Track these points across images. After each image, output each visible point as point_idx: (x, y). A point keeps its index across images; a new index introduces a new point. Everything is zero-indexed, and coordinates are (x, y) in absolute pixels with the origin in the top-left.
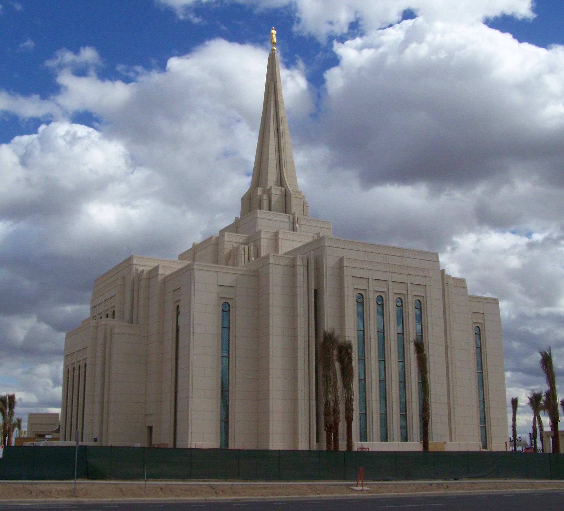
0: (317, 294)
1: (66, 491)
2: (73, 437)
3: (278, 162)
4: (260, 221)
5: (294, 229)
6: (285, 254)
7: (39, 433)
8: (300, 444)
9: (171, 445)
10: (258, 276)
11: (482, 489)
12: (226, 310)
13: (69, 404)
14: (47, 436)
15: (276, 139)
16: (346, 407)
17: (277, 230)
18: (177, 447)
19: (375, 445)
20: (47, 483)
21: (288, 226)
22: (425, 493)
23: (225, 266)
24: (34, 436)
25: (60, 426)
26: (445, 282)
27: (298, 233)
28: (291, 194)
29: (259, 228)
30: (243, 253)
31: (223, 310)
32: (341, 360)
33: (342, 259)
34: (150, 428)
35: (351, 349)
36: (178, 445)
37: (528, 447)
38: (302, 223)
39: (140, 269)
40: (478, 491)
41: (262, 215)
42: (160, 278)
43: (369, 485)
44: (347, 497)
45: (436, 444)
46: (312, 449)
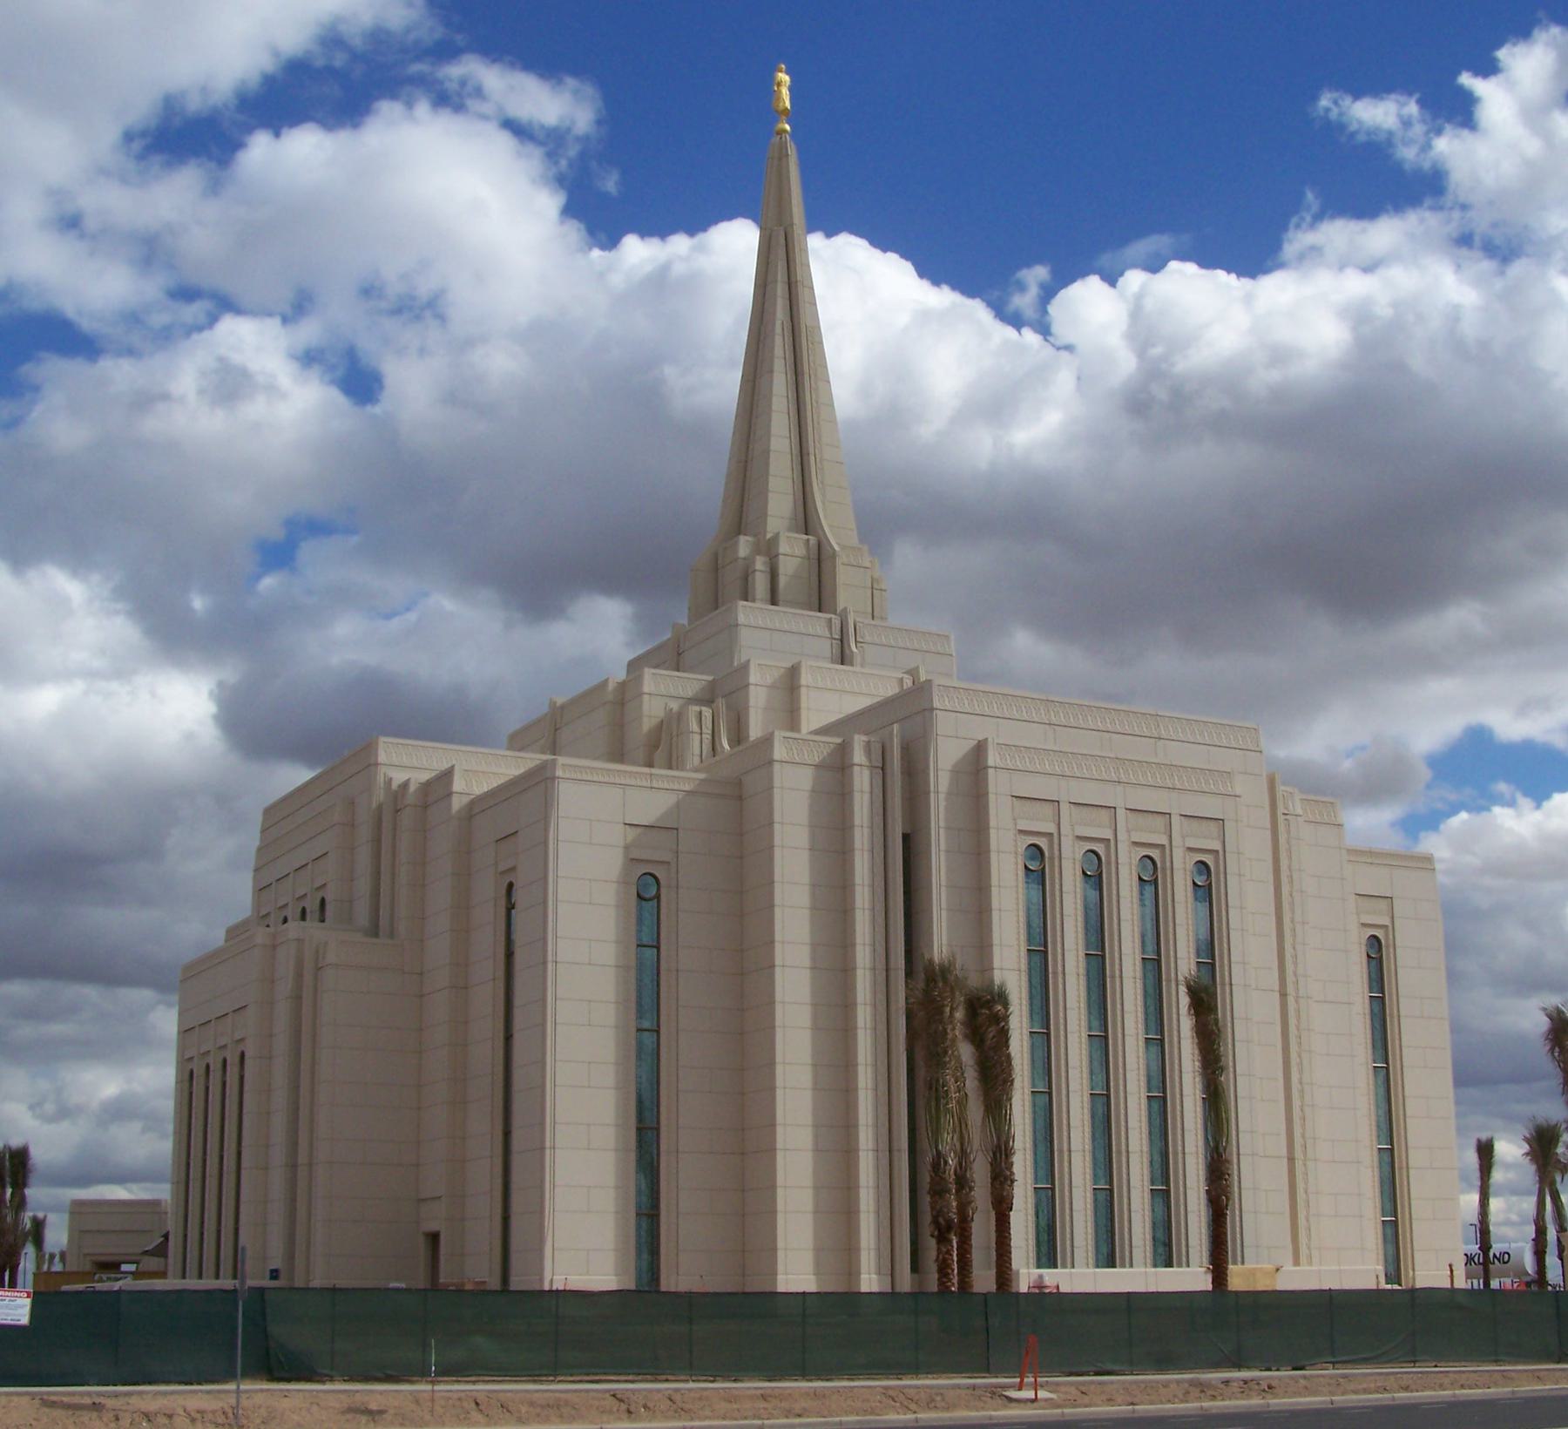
0: (912, 849)
1: (214, 1412)
2: (226, 1265)
3: (797, 460)
4: (745, 636)
5: (843, 658)
6: (817, 732)
7: (103, 1259)
8: (864, 1277)
9: (494, 1283)
10: (740, 798)
11: (1365, 1391)
12: (647, 893)
13: (195, 1173)
14: (124, 1267)
15: (792, 395)
16: (993, 1171)
17: (795, 661)
18: (513, 1287)
19: (1080, 1276)
20: (157, 1393)
21: (826, 647)
22: (1205, 1404)
23: (646, 770)
24: (88, 1267)
25: (166, 1236)
26: (1281, 809)
27: (857, 669)
28: (834, 555)
29: (742, 656)
30: (695, 728)
31: (639, 896)
32: (975, 1035)
33: (980, 749)
34: (434, 1238)
35: (1006, 1005)
36: (516, 1283)
37: (1528, 1279)
38: (868, 638)
39: (399, 777)
40: (1354, 1397)
41: (750, 615)
42: (457, 803)
43: (1054, 1388)
44: (991, 1418)
45: (1253, 1272)
46: (898, 1290)
